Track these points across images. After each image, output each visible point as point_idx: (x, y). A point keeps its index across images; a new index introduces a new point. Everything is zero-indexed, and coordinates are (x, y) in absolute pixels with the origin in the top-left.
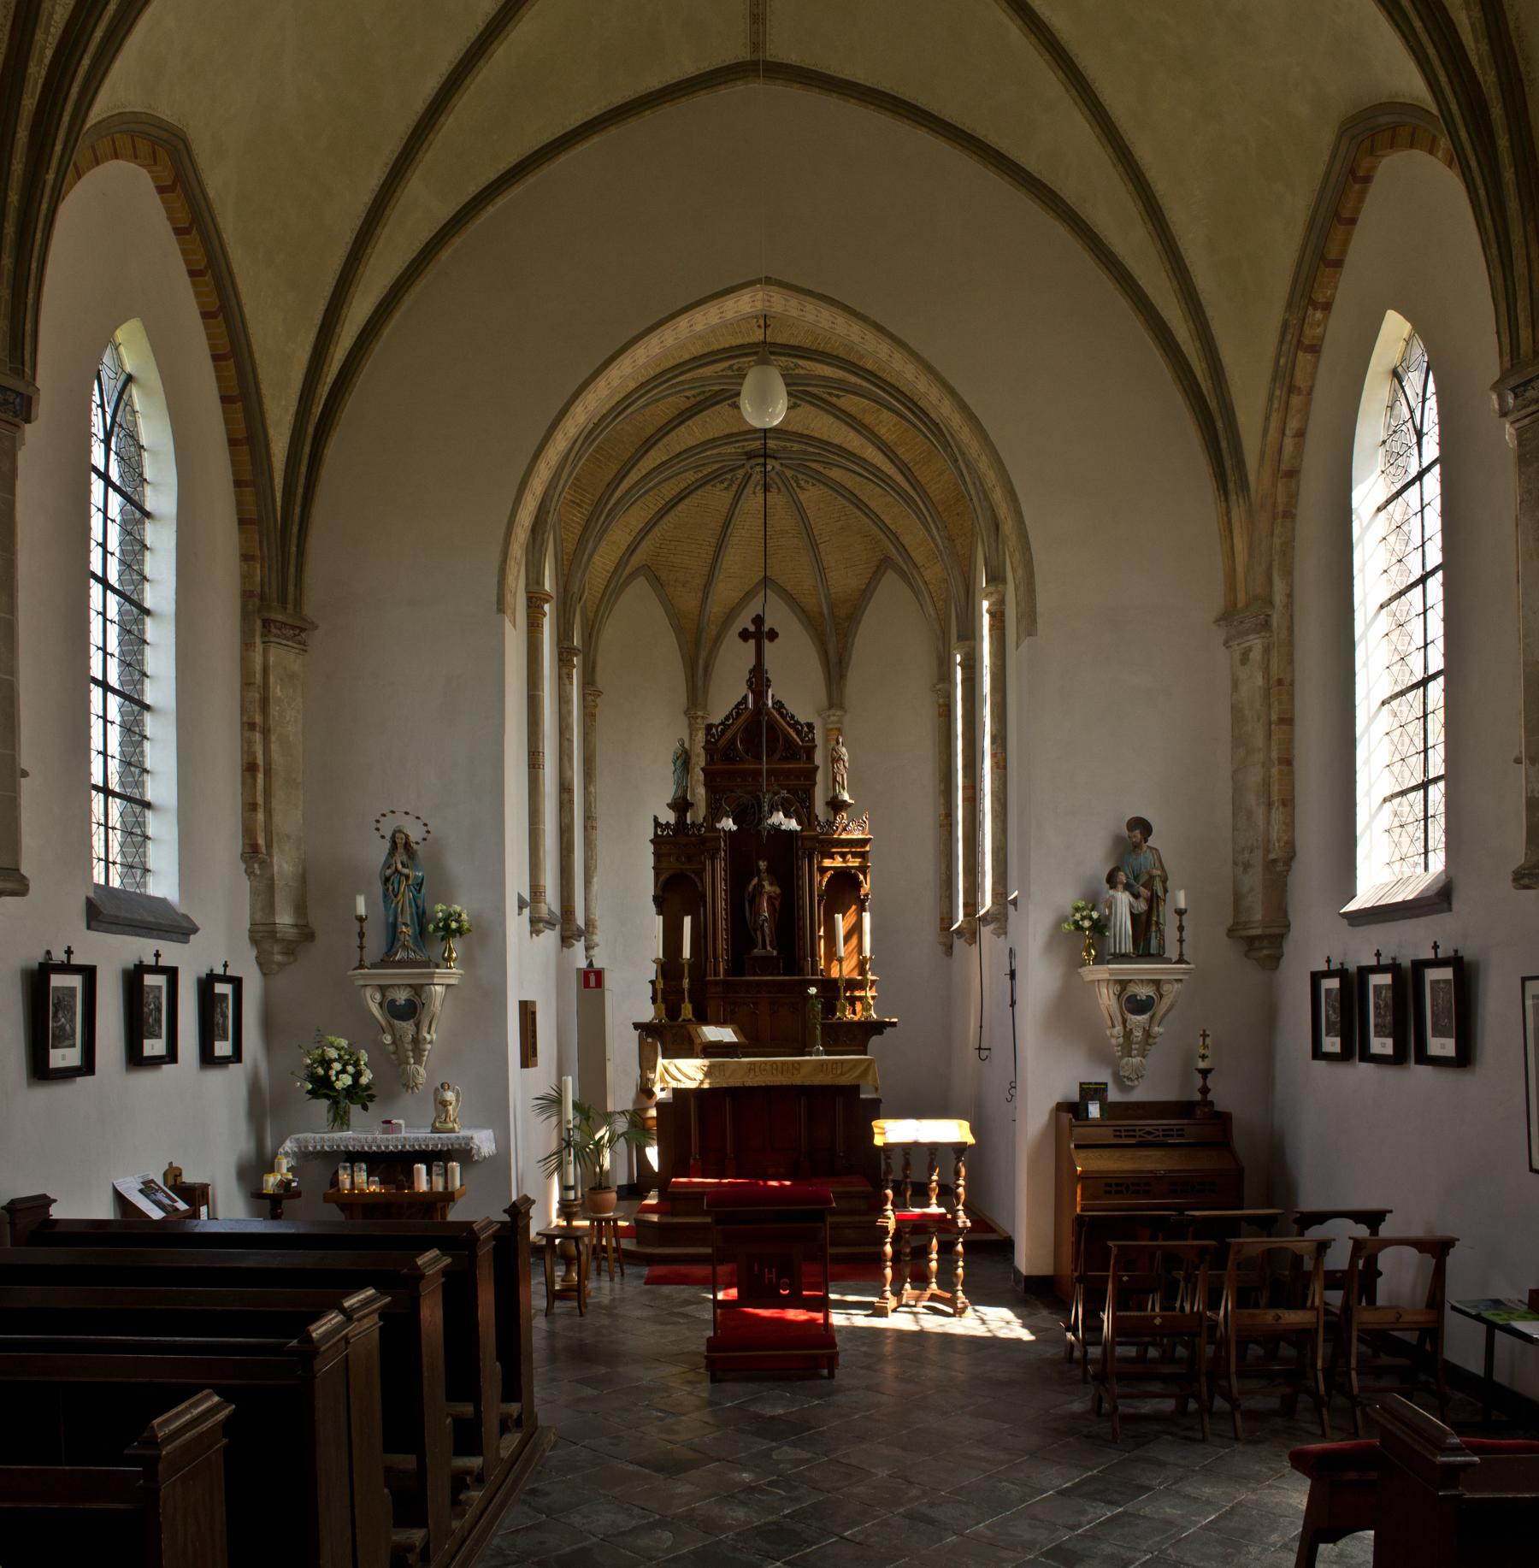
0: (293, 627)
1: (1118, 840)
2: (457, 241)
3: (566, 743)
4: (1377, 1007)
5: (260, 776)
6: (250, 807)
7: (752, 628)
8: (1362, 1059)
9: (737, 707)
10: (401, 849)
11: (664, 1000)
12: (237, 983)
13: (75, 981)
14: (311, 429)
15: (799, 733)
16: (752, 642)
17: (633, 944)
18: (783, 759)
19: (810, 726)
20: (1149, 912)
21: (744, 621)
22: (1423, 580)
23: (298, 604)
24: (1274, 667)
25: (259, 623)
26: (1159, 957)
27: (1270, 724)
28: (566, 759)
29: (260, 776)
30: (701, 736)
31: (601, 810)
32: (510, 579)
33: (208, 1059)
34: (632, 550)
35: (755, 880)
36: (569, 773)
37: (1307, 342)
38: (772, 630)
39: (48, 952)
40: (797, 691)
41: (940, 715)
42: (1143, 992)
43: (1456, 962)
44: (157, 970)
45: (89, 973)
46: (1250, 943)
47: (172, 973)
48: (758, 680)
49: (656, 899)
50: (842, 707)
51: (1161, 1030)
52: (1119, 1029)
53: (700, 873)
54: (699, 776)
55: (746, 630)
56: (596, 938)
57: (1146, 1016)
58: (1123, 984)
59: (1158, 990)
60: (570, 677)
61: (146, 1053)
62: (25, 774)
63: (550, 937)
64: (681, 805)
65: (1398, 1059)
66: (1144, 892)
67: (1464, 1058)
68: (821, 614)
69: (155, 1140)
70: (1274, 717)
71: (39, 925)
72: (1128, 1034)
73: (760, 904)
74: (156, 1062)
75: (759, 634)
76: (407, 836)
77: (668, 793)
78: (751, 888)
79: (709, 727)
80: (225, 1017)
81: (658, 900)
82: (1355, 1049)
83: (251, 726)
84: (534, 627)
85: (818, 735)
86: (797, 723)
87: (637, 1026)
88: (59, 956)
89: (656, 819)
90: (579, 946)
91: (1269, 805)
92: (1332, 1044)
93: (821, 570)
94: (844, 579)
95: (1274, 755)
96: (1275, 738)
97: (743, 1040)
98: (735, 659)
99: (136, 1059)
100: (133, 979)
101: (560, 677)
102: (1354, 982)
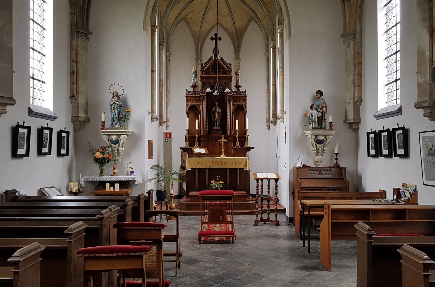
0: (85, 34)
1: (314, 97)
3: (161, 68)
4: (384, 142)
5: (75, 75)
6: (72, 84)
7: (214, 37)
8: (381, 156)
9: (210, 59)
10: (115, 97)
11: (188, 141)
12: (68, 133)
13: (25, 130)
15: (227, 66)
16: (214, 41)
17: (180, 124)
18: (222, 74)
19: (230, 64)
21: (212, 35)
22: (396, 25)
24: (357, 49)
25: (76, 32)
26: (325, 128)
27: (355, 64)
29: (75, 75)
30: (200, 67)
32: (147, 21)
33: (59, 154)
34: (180, 14)
35: (214, 108)
38: (220, 37)
39: (18, 122)
40: (227, 54)
42: (321, 138)
43: (403, 128)
44: (47, 128)
45: (29, 128)
46: (351, 125)
47: (51, 130)
48: (216, 51)
50: (239, 59)
51: (327, 149)
52: (315, 148)
53: (199, 105)
54: (199, 78)
55: (212, 37)
57: (322, 145)
58: (316, 136)
59: (325, 138)
61: (43, 152)
62: (14, 72)
63: (157, 123)
65: (389, 156)
66: (320, 111)
67: (406, 155)
68: (233, 33)
69: (45, 177)
70: (356, 62)
71: (15, 115)
73: (216, 115)
74: (45, 154)
75: (216, 38)
76: (117, 93)
77: (192, 83)
78: (213, 110)
79: (202, 64)
80: (64, 143)
81: (188, 113)
82: (379, 154)
83: (73, 61)
85: (233, 67)
86: (227, 63)
87: (181, 148)
88: (21, 123)
90: (164, 126)
91: (355, 86)
92: (373, 152)
93: (234, 23)
94: (240, 24)
95: (356, 73)
96: (357, 68)
97: (207, 152)
98: (209, 46)
99: (40, 153)
100: (40, 131)
101: (160, 49)
102: (377, 135)
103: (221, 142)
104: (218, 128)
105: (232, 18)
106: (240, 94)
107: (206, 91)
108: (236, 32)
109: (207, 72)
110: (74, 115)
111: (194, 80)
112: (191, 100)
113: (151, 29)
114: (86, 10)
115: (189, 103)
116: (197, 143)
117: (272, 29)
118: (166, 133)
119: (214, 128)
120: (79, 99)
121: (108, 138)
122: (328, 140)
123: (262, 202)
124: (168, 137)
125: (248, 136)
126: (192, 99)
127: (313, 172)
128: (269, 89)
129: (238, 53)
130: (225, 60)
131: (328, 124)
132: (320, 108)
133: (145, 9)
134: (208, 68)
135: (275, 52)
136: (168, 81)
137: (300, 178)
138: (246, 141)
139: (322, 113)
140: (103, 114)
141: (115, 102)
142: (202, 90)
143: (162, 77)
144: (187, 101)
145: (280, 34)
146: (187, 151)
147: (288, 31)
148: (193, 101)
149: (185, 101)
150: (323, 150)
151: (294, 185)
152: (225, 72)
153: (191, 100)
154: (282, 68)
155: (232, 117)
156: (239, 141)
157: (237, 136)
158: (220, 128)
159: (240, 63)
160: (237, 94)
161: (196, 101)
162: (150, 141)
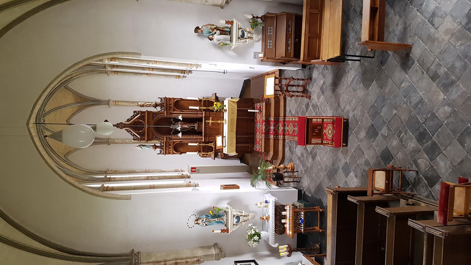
1: (199, 35)
2: (12, 218)
3: (134, 179)
9: (128, 132)
10: (198, 222)
14: (71, 256)
15: (136, 115)
18: (144, 120)
20: (220, 30)
23: (127, 255)
28: (139, 179)
29: (178, 261)
42: (240, 33)
49: (180, 154)
50: (109, 101)
52: (247, 40)
53: (174, 143)
56: (179, 169)
57: (245, 33)
58: (239, 38)
60: (114, 178)
64: (155, 147)
66: (215, 31)
72: (249, 38)
77: (151, 149)
84: (113, 189)
86: (133, 115)
93: (70, 105)
94: (70, 99)
104: (196, 125)
105: (65, 106)
106: (164, 103)
107: (112, 132)
108: (79, 103)
109: (142, 135)
110: (214, 258)
113: (107, 191)
115: (171, 152)
116: (212, 145)
118: (192, 171)
119: (196, 128)
123: (289, 91)
124: (195, 170)
126: (167, 149)
127: (268, 44)
128: (147, 74)
129: (101, 102)
131: (227, 25)
133: (108, 200)
134: (139, 134)
136: (138, 171)
138: (208, 100)
139: (218, 30)
144: (169, 153)
145: (111, 60)
146: (218, 153)
150: (249, 32)
151: (276, 62)
152: (142, 117)
155: (186, 112)
159: (112, 99)
160: (164, 106)
161: (170, 145)
162: (224, 188)
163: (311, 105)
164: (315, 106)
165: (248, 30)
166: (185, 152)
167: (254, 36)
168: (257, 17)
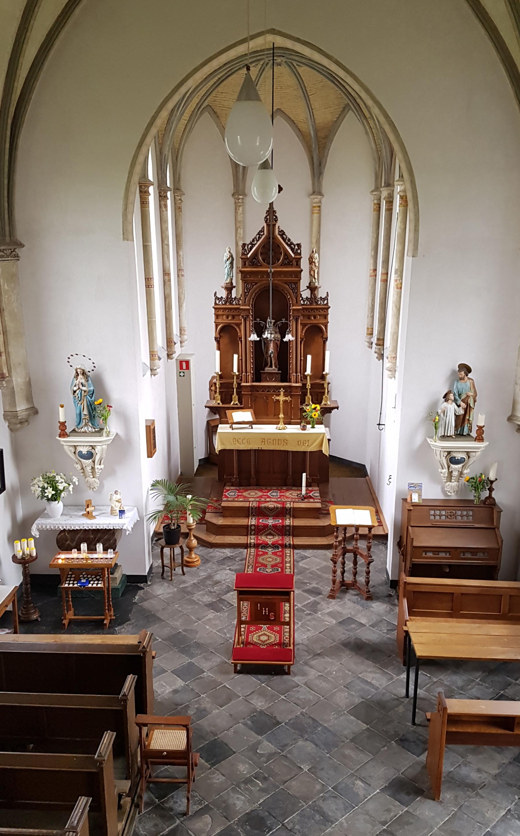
1: (454, 373)
3: (165, 247)
9: (259, 234)
10: (80, 376)
18: (283, 265)
19: (299, 245)
20: (465, 415)
28: (166, 256)
31: (187, 265)
36: (167, 265)
37: (450, 776)
41: (374, 210)
49: (216, 339)
50: (320, 193)
52: (445, 470)
53: (238, 325)
56: (185, 337)
57: (460, 466)
64: (229, 288)
66: (463, 405)
68: (310, 135)
72: (450, 473)
76: (83, 370)
77: (224, 280)
84: (144, 203)
86: (292, 243)
89: (215, 293)
94: (324, 116)
103: (278, 401)
106: (317, 304)
109: (253, 261)
110: (8, 409)
111: (228, 275)
112: (223, 315)
113: (141, 192)
114: (6, 199)
115: (220, 321)
116: (235, 401)
117: (389, 160)
118: (181, 362)
120: (14, 379)
121: (73, 450)
122: (470, 459)
123: (344, 554)
124: (184, 367)
125: (329, 384)
126: (226, 312)
128: (375, 270)
130: (289, 236)
131: (475, 429)
132: (463, 397)
133: (122, 195)
135: (391, 209)
136: (181, 253)
137: (412, 526)
138: (323, 393)
140: (60, 408)
141: (81, 386)
142: (243, 296)
143: (167, 264)
144: (217, 316)
146: (218, 414)
147: (413, 227)
148: (227, 317)
149: (213, 316)
150: (461, 474)
153: (223, 315)
154: (400, 272)
156: (311, 394)
157: (309, 386)
158: (276, 371)
159: (323, 200)
160: (311, 304)
161: (233, 317)
163: (317, 598)
164: (314, 607)
165: (465, 471)
166: (219, 348)
167: (454, 484)
168: (491, 490)
